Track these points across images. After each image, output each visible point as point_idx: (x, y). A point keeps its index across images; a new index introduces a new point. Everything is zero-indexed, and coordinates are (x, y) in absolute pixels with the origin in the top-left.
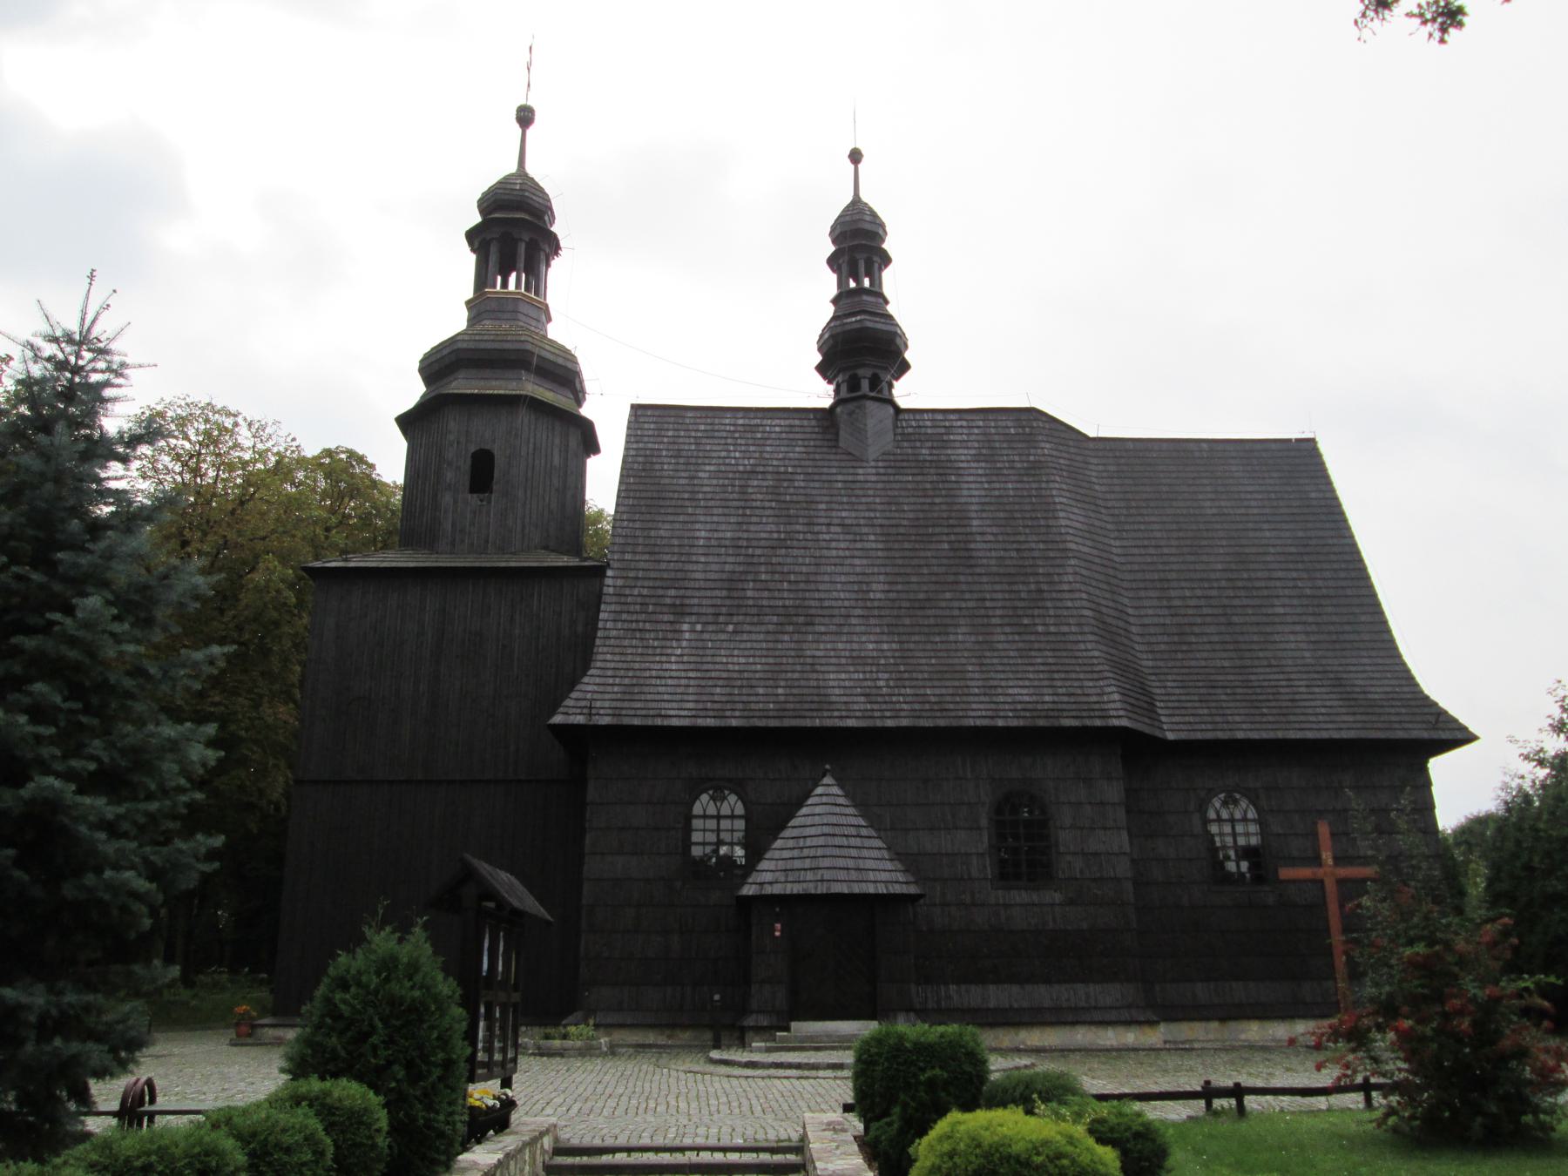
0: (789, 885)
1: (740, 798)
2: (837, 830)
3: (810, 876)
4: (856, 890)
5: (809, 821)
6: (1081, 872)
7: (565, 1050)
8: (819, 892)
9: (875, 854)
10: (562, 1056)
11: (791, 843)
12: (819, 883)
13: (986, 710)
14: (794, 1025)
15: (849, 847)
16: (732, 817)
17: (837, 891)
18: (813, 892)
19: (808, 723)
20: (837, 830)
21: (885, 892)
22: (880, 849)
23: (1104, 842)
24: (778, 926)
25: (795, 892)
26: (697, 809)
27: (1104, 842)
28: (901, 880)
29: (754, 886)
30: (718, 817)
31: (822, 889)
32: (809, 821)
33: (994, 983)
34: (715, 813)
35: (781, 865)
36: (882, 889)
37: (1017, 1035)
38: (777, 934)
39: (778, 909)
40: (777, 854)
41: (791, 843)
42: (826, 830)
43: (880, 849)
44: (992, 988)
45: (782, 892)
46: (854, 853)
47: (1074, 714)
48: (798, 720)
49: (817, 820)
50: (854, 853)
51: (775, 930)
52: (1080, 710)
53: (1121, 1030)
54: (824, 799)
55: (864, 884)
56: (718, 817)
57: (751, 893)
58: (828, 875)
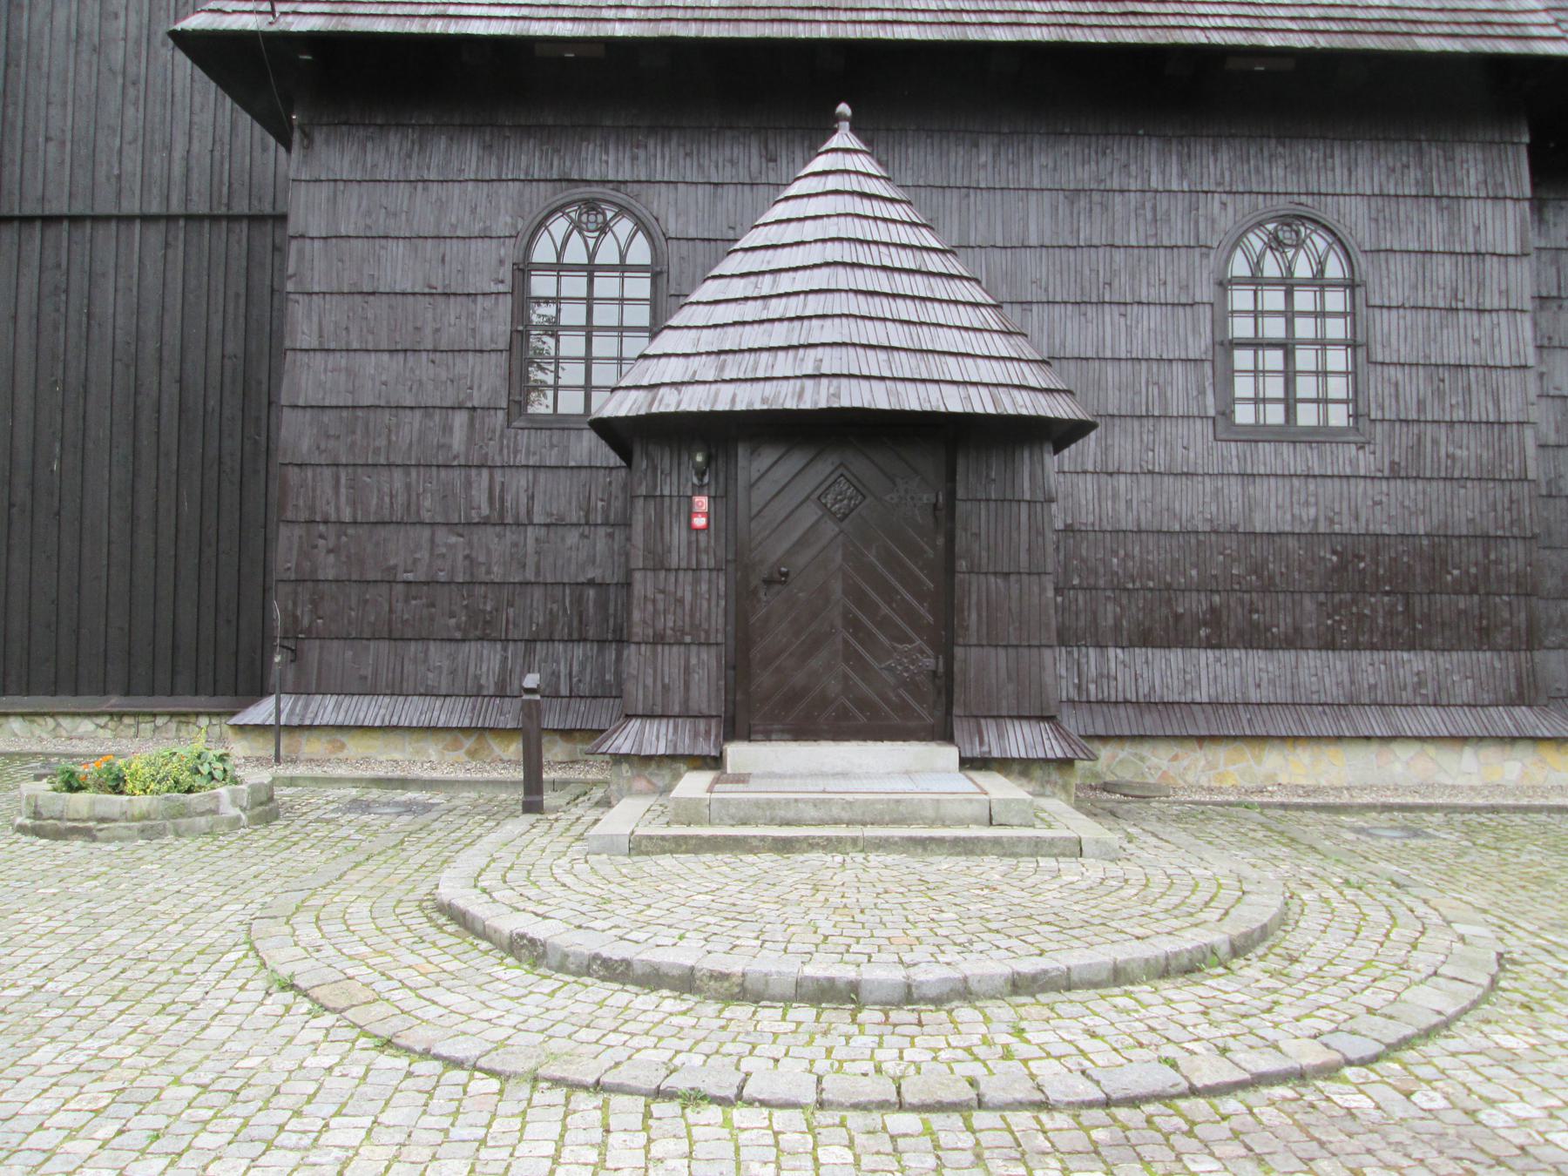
0: (728, 390)
1: (641, 225)
2: (863, 255)
3: (784, 364)
4: (913, 404)
5: (790, 233)
6: (1421, 405)
7: (102, 820)
8: (807, 405)
9: (966, 316)
10: (89, 835)
11: (739, 288)
12: (809, 383)
13: (1233, 16)
14: (738, 754)
15: (895, 296)
16: (622, 268)
17: (857, 404)
18: (791, 404)
19: (802, 32)
20: (863, 255)
21: (991, 410)
22: (976, 305)
23: (1477, 342)
24: (702, 503)
25: (740, 406)
26: (543, 251)
27: (1477, 342)
28: (1033, 383)
29: (634, 394)
30: (591, 269)
31: (816, 397)
32: (790, 233)
33: (1209, 645)
34: (585, 261)
35: (709, 340)
36: (981, 403)
37: (1259, 762)
38: (700, 522)
39: (699, 458)
40: (698, 315)
41: (739, 288)
42: (834, 252)
43: (976, 305)
44: (1206, 657)
45: (706, 408)
46: (905, 310)
47: (1446, 29)
48: (776, 26)
49: (810, 230)
50: (905, 310)
51: (691, 514)
52: (1458, 23)
53: (1490, 754)
54: (832, 183)
55: (932, 388)
56: (591, 269)
57: (622, 413)
58: (832, 361)
